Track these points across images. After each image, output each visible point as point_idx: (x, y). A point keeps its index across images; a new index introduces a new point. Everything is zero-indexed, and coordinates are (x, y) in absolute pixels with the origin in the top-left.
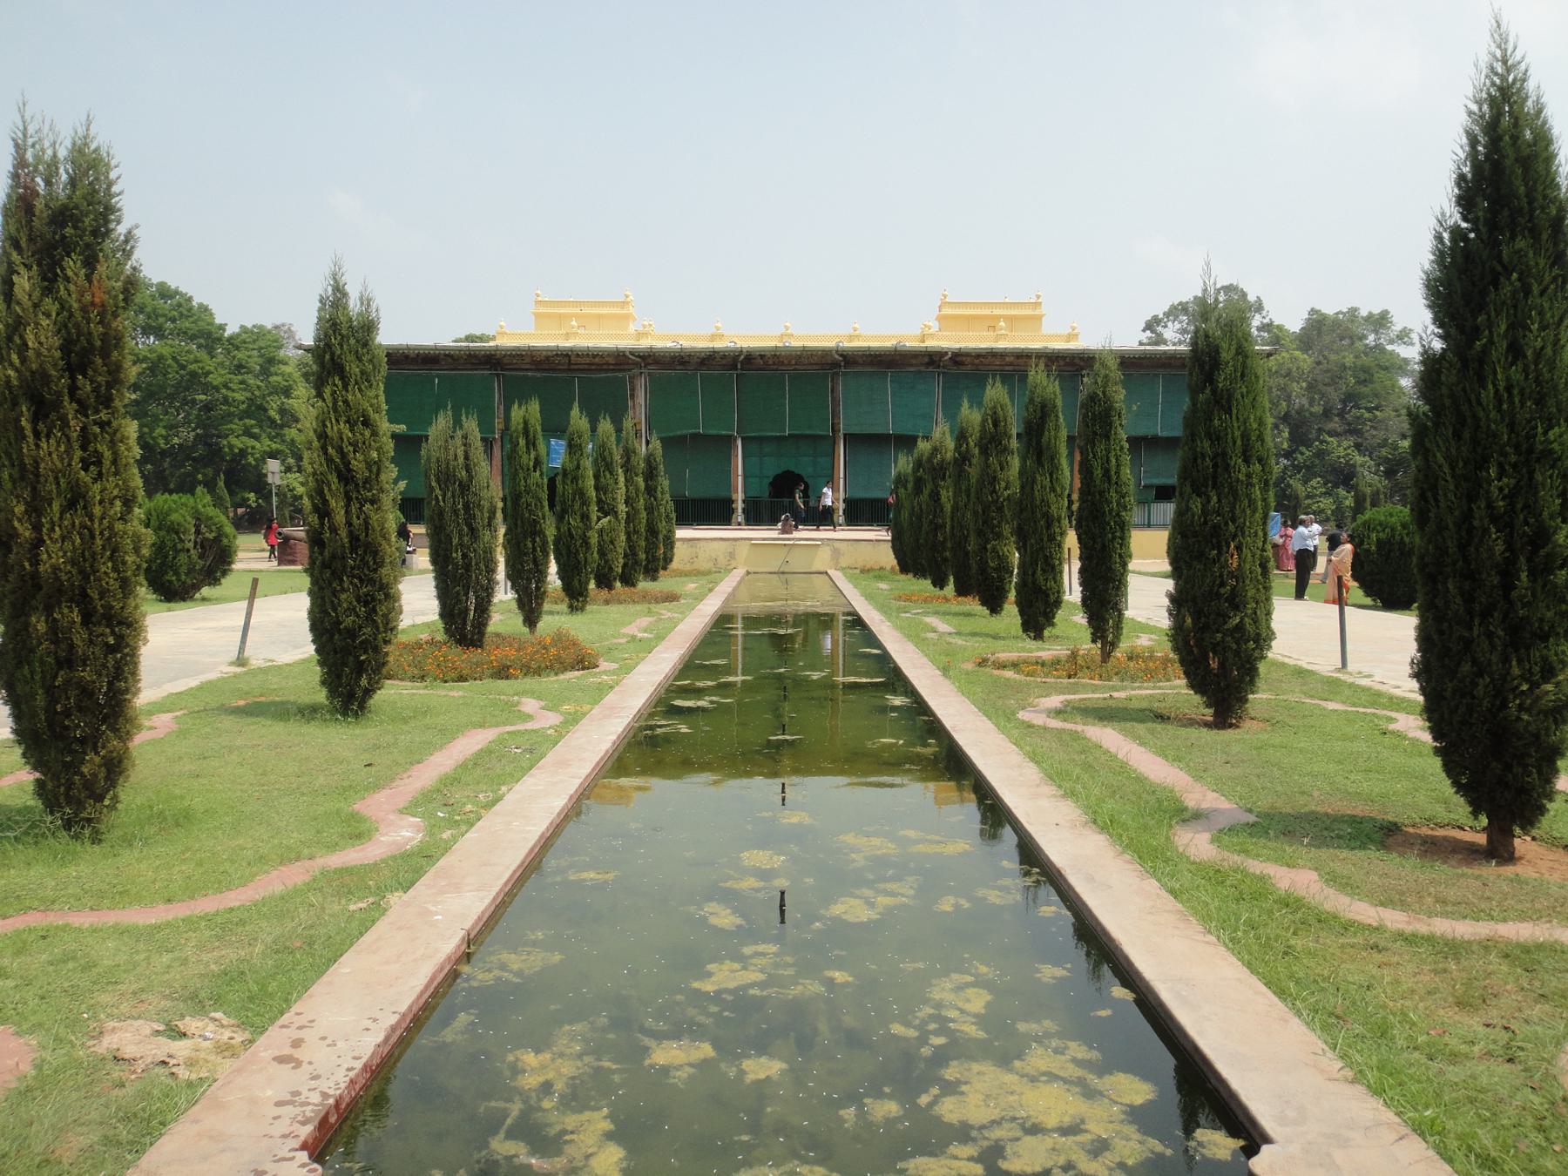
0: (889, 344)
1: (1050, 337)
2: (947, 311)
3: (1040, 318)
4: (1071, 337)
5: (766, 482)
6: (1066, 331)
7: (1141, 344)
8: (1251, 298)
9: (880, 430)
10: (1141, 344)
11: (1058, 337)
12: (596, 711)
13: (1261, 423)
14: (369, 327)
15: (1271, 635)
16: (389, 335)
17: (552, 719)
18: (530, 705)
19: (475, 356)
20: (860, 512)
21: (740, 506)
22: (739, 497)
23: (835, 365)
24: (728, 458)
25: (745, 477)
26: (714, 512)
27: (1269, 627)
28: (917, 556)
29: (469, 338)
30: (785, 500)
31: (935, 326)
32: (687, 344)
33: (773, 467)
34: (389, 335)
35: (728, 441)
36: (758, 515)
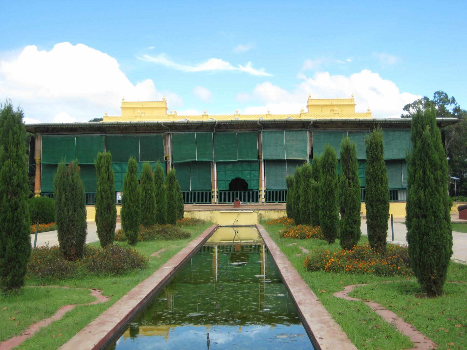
0: (284, 118)
1: (358, 114)
2: (311, 103)
3: (354, 105)
4: (369, 113)
5: (228, 183)
6: (366, 111)
7: (402, 116)
8: (450, 97)
9: (280, 158)
10: (402, 116)
11: (362, 114)
12: (125, 296)
13: (163, 175)
14: (21, 116)
15: (452, 253)
16: (28, 120)
17: (105, 300)
18: (96, 294)
19: (93, 127)
20: (273, 196)
21: (215, 194)
22: (215, 190)
23: (259, 128)
24: (210, 172)
25: (218, 181)
26: (203, 197)
27: (451, 249)
28: (301, 215)
29: (96, 120)
30: (239, 192)
31: (306, 110)
32: (191, 120)
33: (231, 177)
34: (28, 120)
35: (209, 164)
36: (223, 198)
